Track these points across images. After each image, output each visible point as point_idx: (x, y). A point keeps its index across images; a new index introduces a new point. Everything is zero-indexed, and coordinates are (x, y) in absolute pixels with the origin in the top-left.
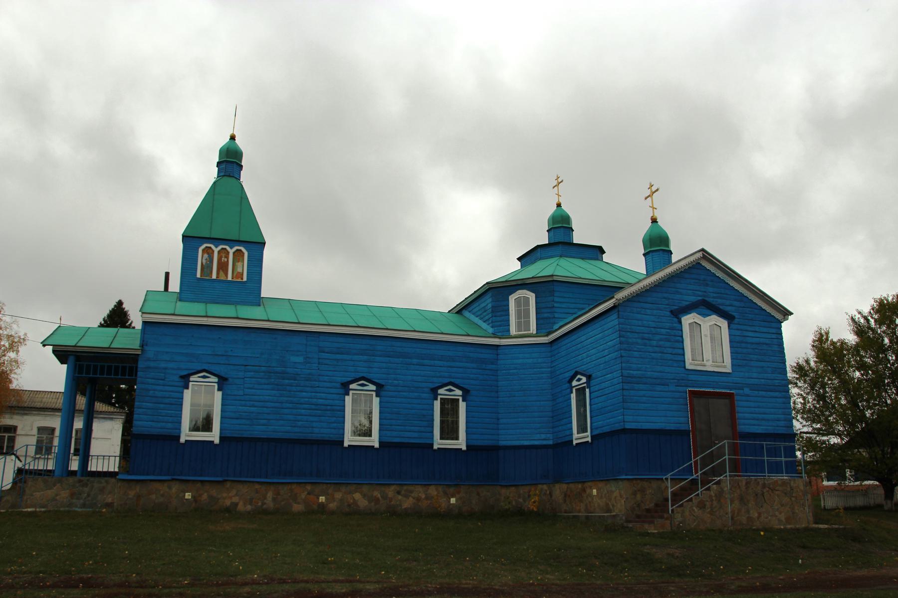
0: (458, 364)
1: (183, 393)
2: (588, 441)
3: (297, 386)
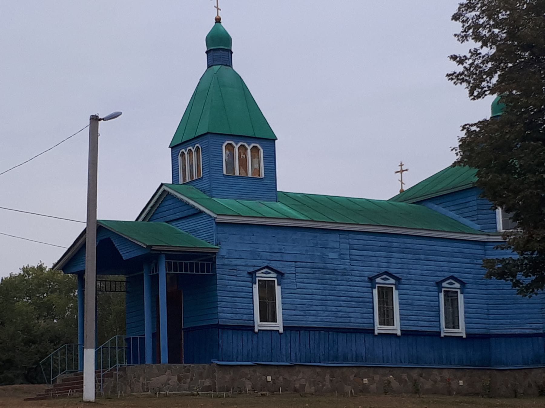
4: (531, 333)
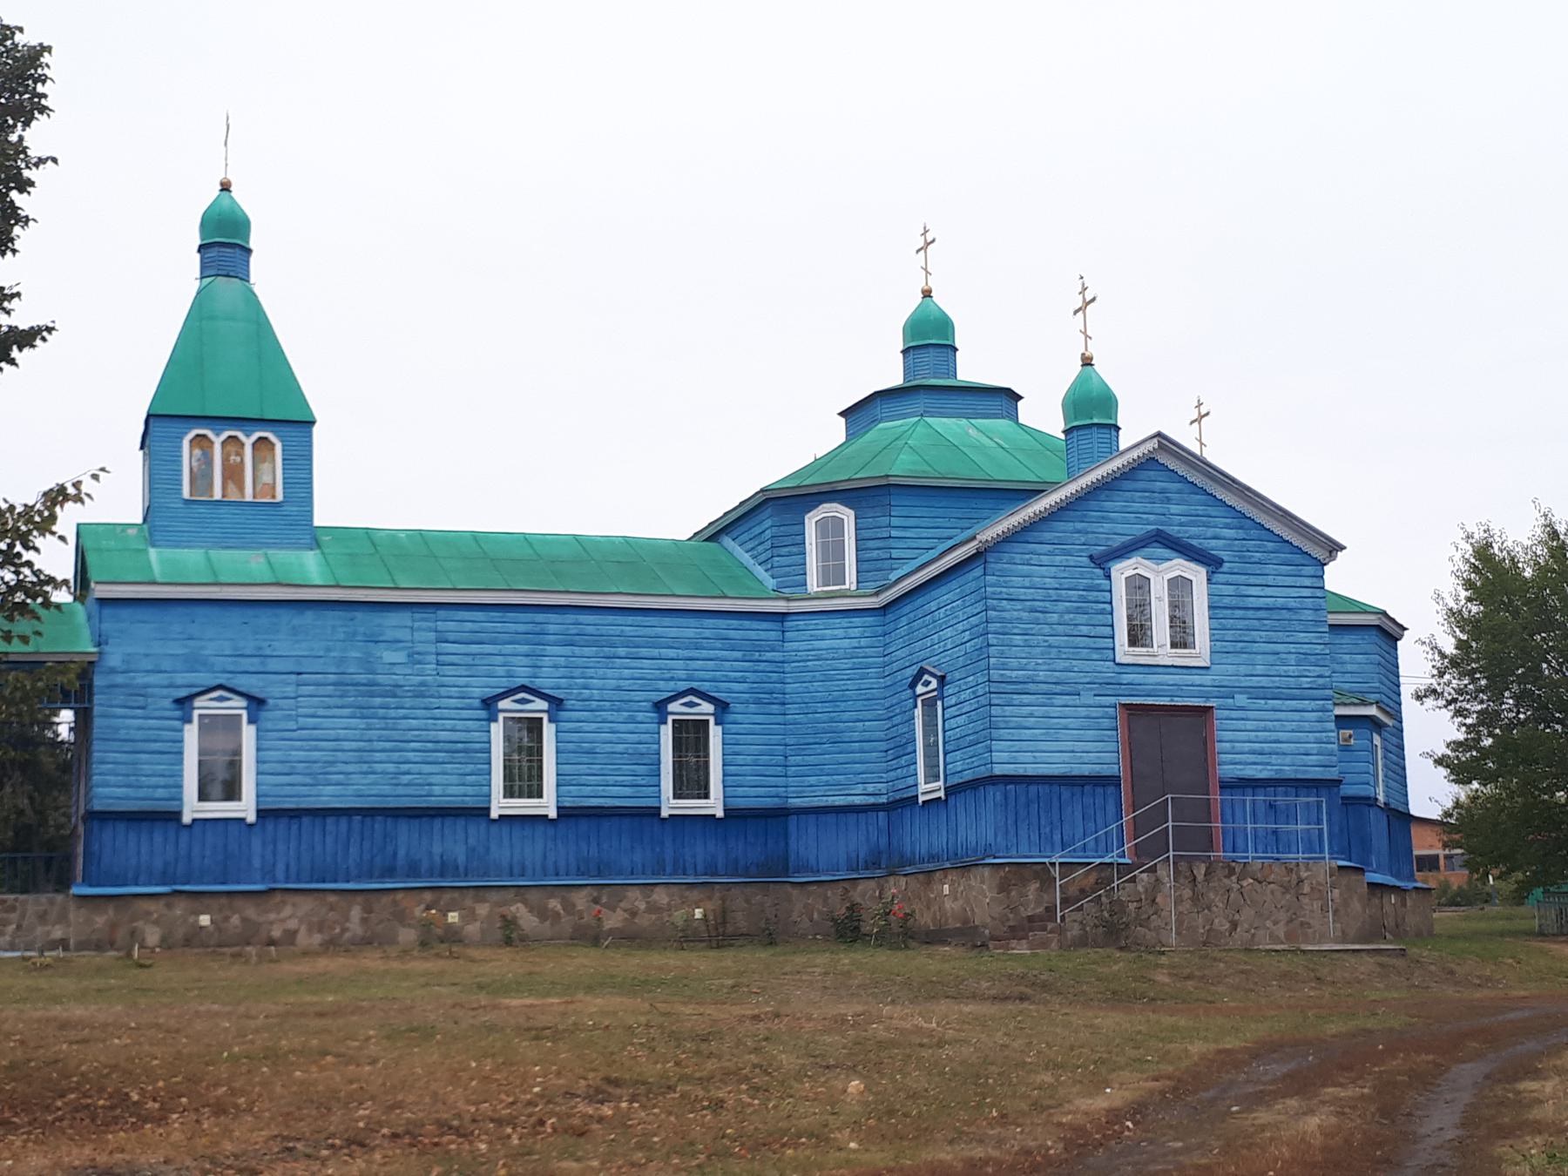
0: (705, 653)
1: (181, 730)
2: (940, 798)
3: (397, 708)
4: (864, 802)
